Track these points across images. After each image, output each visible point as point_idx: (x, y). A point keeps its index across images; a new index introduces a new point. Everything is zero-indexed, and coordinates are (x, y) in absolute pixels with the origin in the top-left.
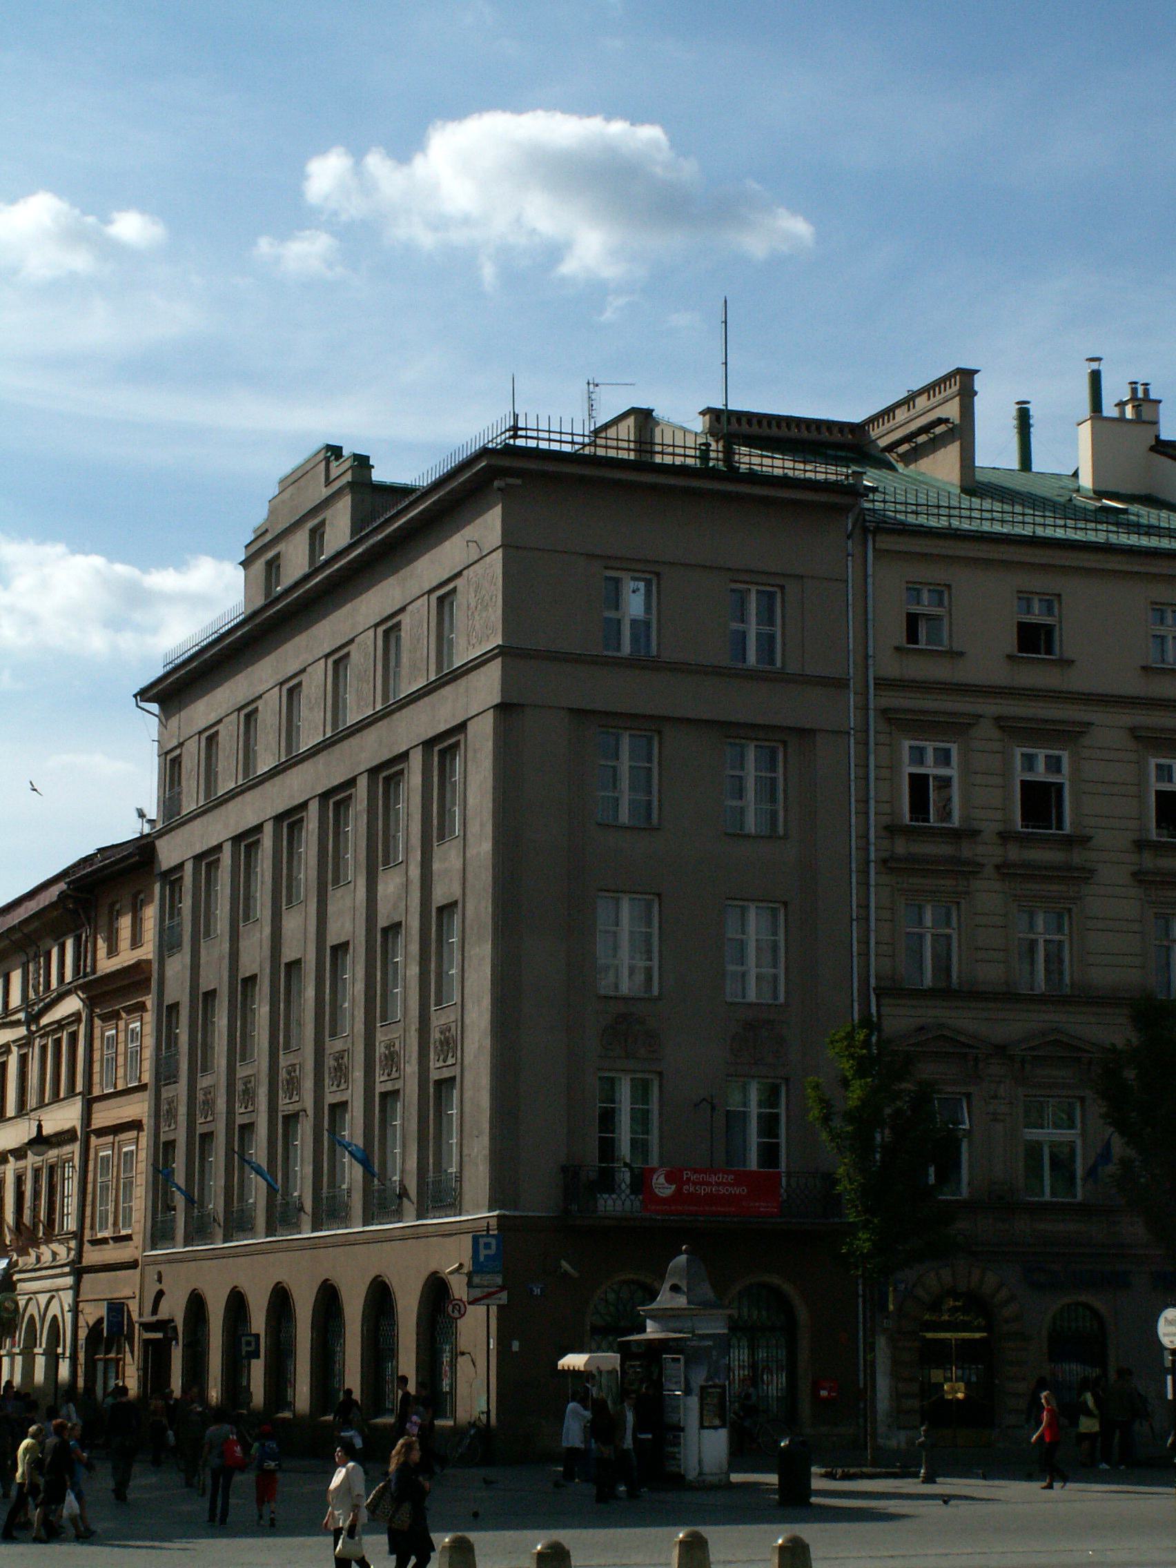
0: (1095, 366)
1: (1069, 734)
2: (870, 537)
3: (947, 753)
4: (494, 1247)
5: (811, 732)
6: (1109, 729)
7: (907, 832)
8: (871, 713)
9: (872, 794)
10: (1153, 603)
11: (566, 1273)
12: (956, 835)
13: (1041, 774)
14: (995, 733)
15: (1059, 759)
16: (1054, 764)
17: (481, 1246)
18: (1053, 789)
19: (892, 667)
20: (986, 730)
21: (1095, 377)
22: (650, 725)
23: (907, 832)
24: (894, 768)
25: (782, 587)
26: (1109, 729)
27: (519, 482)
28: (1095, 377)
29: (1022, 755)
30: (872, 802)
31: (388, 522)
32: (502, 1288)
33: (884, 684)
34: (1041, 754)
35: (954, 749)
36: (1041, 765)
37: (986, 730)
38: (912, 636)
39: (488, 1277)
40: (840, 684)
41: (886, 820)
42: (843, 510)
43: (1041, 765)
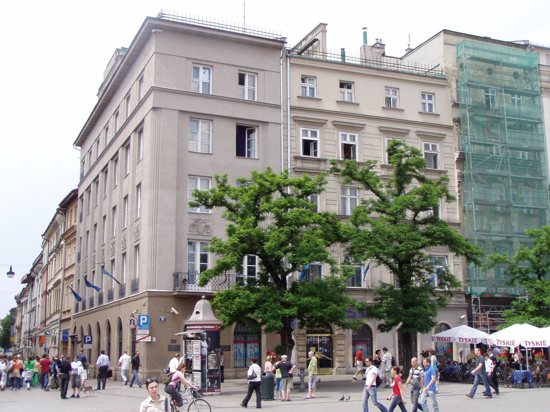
0: (365, 30)
1: (359, 128)
2: (288, 59)
3: (316, 132)
4: (146, 319)
5: (268, 122)
6: (372, 128)
7: (302, 159)
8: (289, 117)
9: (289, 145)
10: (385, 87)
11: (173, 313)
12: (319, 160)
13: (348, 141)
14: (333, 127)
15: (354, 136)
16: (353, 138)
17: (141, 319)
18: (352, 148)
19: (297, 103)
20: (329, 125)
21: (365, 34)
22: (209, 118)
23: (302, 159)
24: (297, 137)
25: (257, 74)
26: (372, 128)
27: (161, 31)
28: (365, 34)
29: (342, 135)
30: (289, 148)
31: (114, 76)
32: (149, 335)
33: (293, 108)
34: (348, 135)
35: (318, 132)
36: (348, 138)
37: (329, 125)
38: (306, 151)
39: (144, 331)
40: (278, 107)
41: (294, 155)
42: (280, 48)
43: (348, 138)
